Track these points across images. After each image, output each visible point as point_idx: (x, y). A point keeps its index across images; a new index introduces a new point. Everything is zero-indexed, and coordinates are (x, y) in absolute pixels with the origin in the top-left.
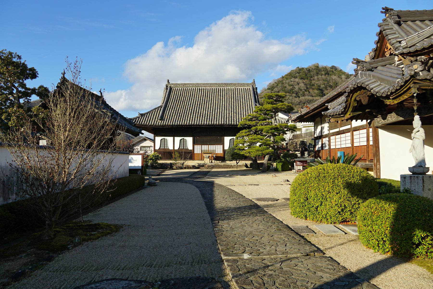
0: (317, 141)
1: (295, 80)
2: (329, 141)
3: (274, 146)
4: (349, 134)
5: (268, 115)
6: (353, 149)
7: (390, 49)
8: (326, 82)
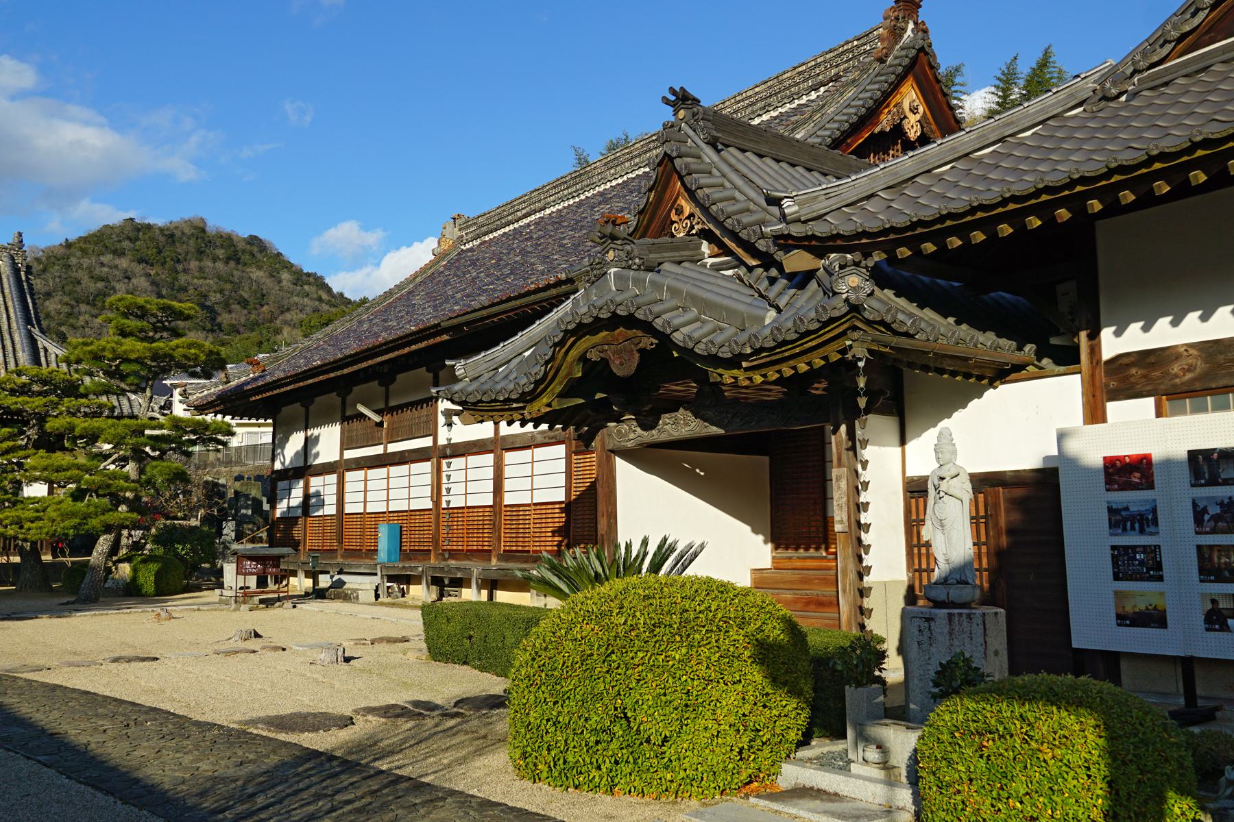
0: (281, 485)
1: (117, 262)
2: (341, 484)
3: (138, 498)
4: (427, 466)
5: (123, 378)
6: (438, 515)
7: (691, 215)
8: (228, 286)
